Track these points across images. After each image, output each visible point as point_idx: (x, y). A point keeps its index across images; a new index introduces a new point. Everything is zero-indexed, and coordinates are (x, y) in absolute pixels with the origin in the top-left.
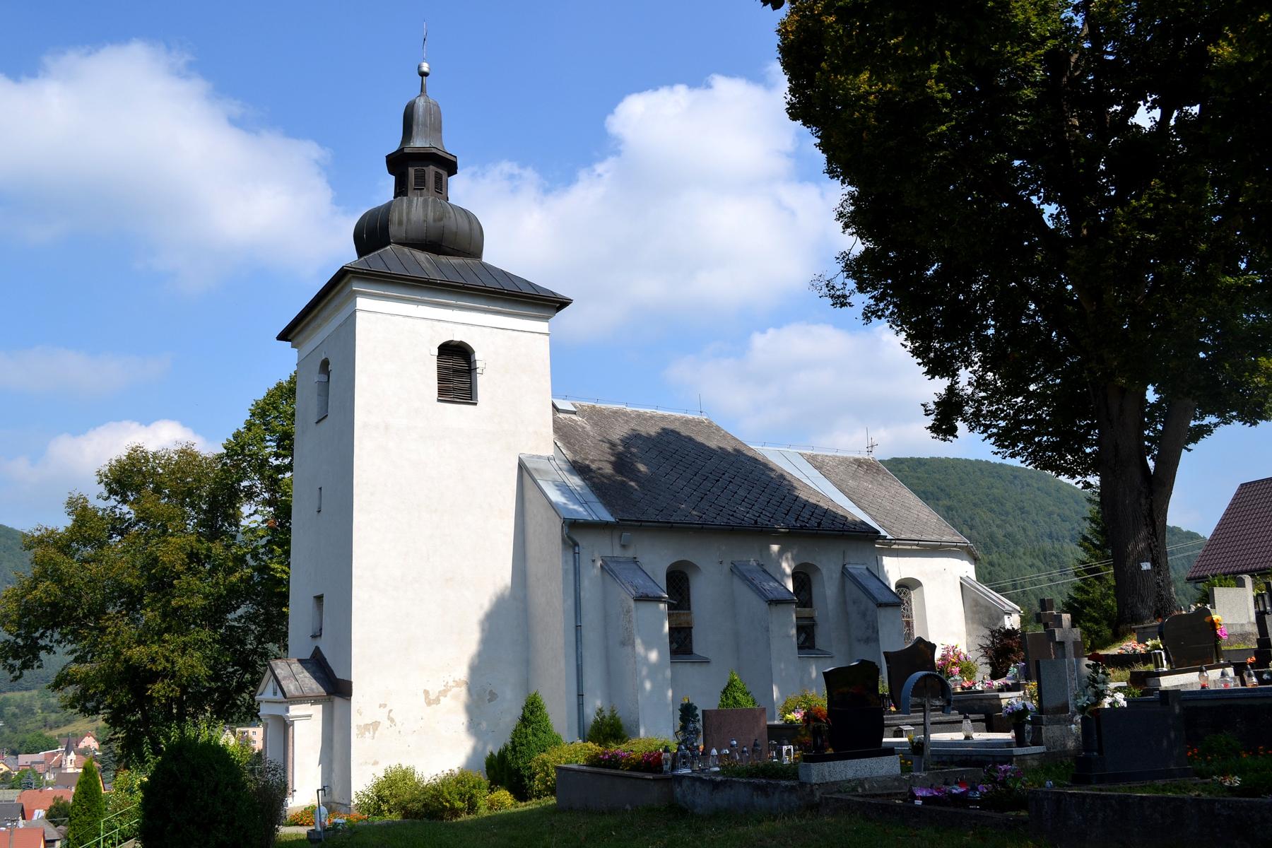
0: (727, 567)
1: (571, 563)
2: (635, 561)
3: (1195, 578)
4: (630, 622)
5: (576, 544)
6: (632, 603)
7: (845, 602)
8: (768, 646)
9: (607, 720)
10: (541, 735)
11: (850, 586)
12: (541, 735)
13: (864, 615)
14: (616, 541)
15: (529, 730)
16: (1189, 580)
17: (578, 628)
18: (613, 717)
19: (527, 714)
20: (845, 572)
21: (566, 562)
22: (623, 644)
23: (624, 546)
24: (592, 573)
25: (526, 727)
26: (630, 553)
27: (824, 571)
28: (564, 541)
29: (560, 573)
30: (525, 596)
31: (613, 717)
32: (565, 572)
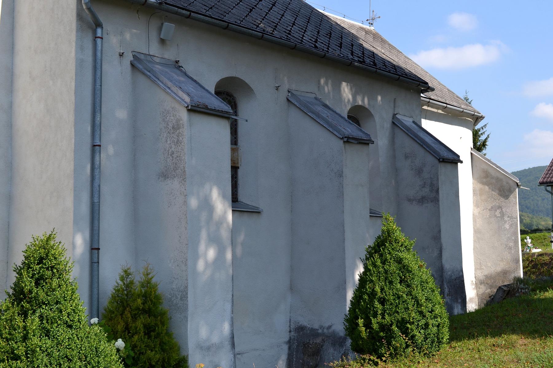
0: (283, 94)
1: (89, 52)
2: (177, 65)
3: (546, 183)
4: (178, 142)
5: (98, 24)
6: (184, 115)
7: (394, 157)
8: (341, 195)
9: (137, 288)
10: (63, 333)
11: (401, 138)
12: (63, 333)
13: (419, 172)
14: (154, 35)
15: (33, 322)
16: (542, 183)
17: (95, 148)
18: (147, 284)
19: (28, 284)
20: (395, 124)
21: (80, 48)
22: (164, 175)
23: (163, 42)
24: (116, 73)
25: (24, 314)
26: (170, 54)
27: (377, 118)
28: (80, 17)
29: (72, 66)
30: (11, 105)
31: (147, 284)
32: (80, 64)
